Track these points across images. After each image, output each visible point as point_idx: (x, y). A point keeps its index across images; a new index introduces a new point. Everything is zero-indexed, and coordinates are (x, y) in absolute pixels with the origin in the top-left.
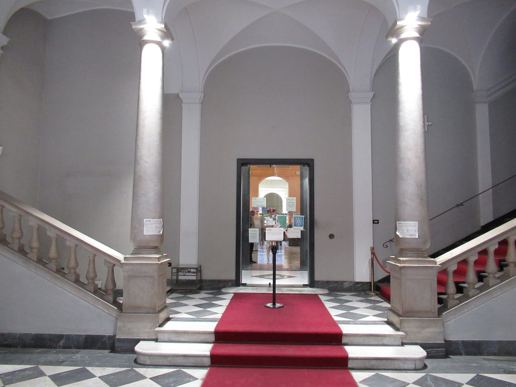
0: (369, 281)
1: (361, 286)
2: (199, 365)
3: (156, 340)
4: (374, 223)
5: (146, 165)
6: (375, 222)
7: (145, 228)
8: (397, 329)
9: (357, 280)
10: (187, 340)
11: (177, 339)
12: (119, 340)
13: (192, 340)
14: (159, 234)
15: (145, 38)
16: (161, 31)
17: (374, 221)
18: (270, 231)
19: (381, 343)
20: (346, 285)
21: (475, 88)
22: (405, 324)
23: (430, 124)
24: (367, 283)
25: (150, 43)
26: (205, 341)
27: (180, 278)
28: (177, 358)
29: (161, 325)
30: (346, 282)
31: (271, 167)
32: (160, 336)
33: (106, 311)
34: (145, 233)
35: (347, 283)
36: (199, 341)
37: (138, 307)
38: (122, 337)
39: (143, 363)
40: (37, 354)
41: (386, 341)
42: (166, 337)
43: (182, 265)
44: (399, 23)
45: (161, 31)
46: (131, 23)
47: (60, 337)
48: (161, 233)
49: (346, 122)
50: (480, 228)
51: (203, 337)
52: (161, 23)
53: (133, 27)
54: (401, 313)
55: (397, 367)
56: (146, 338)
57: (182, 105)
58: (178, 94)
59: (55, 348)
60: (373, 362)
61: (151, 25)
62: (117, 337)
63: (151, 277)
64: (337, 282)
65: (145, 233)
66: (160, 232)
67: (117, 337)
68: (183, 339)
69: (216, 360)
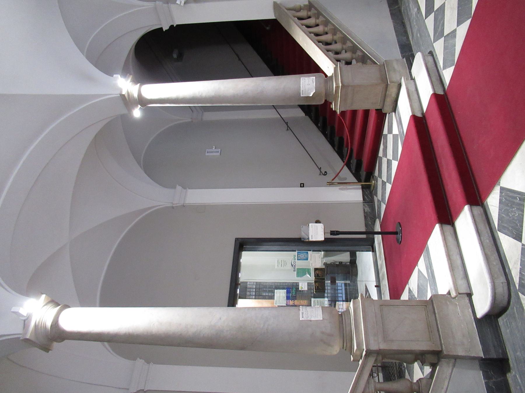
0: (361, 191)
1: (368, 197)
3: (470, 295)
4: (303, 187)
6: (302, 185)
7: (313, 319)
8: (400, 86)
9: (361, 199)
10: (458, 257)
11: (460, 268)
12: (485, 350)
13: (457, 250)
15: (49, 324)
17: (301, 187)
18: (313, 236)
19: (415, 92)
20: (367, 209)
21: (190, 120)
22: (394, 79)
23: (214, 147)
24: (363, 191)
25: (58, 318)
26: (454, 235)
28: (484, 244)
30: (364, 210)
31: (240, 284)
33: (446, 384)
34: (320, 318)
35: (366, 209)
36: (456, 243)
37: (429, 326)
39: (506, 288)
41: (412, 89)
42: (462, 283)
44: (124, 93)
49: (202, 209)
50: (307, 117)
51: (450, 239)
52: (41, 296)
54: (384, 85)
55: (433, 66)
60: (434, 79)
61: (37, 311)
62: (482, 355)
64: (365, 217)
65: (320, 318)
67: (482, 355)
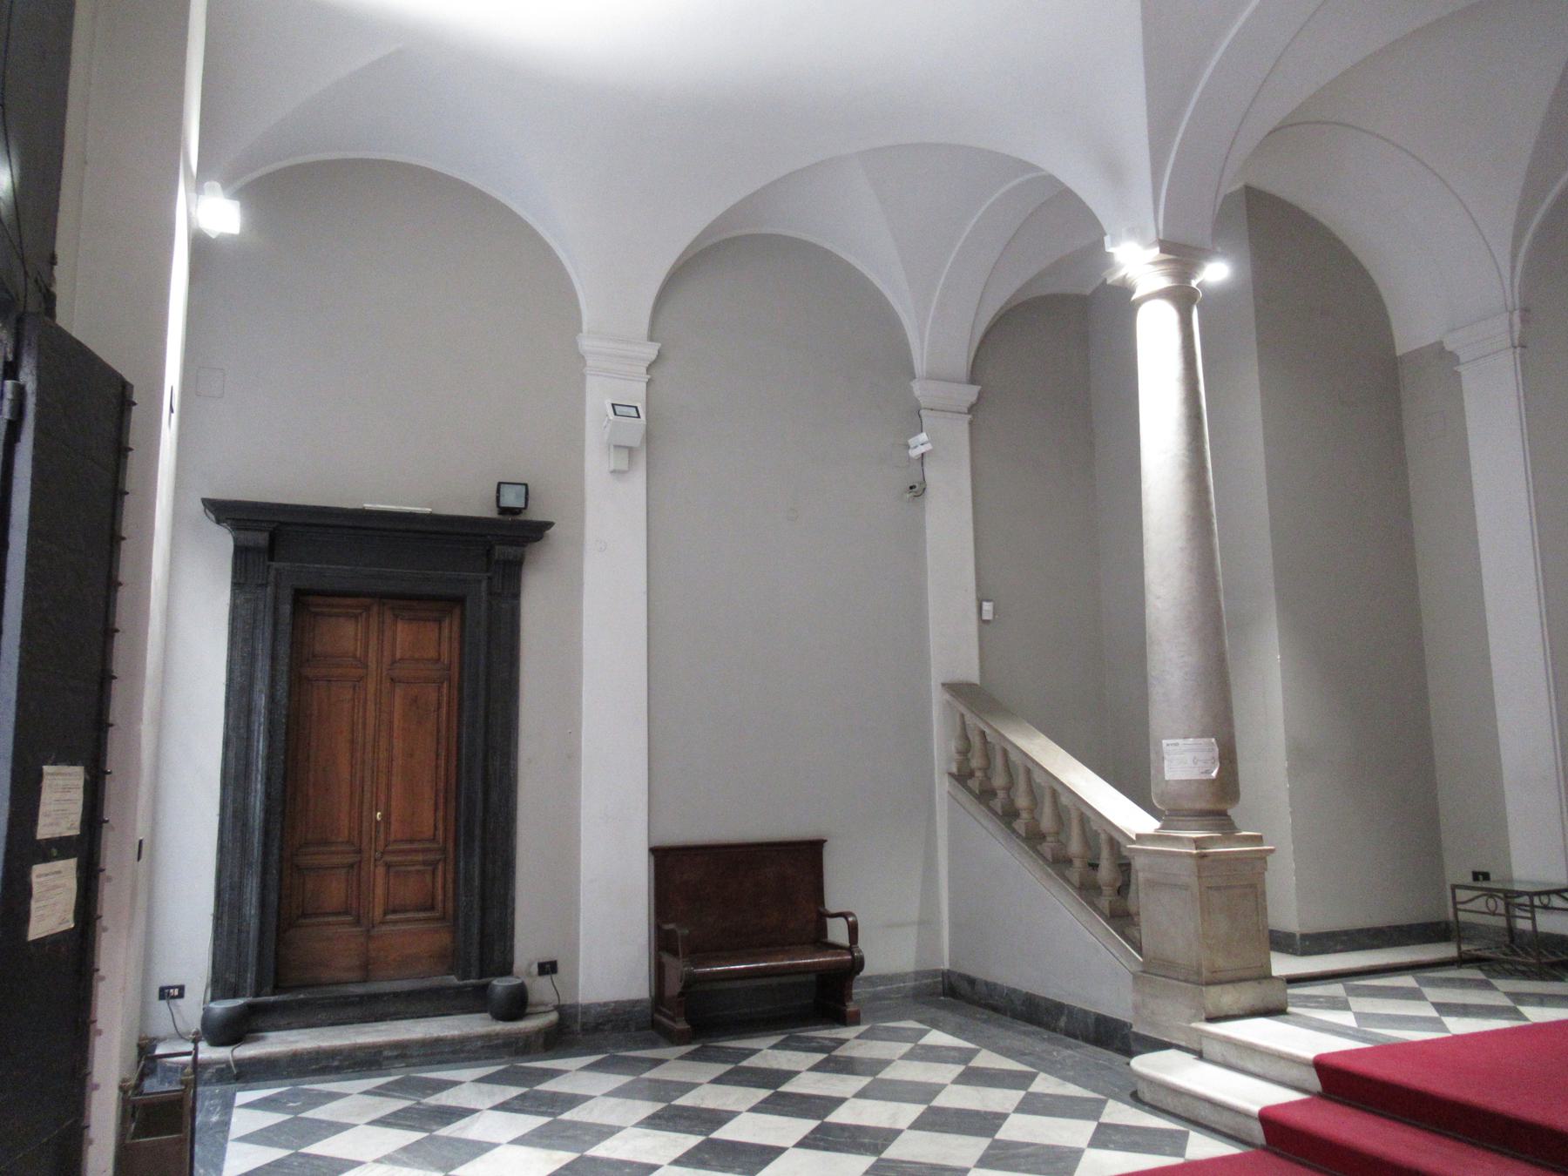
2: (1243, 1136)
5: (1159, 604)
11: (1241, 1063)
13: (1286, 1079)
14: (1204, 777)
16: (1155, 263)
27: (1523, 924)
29: (1211, 1019)
32: (1209, 1048)
38: (1142, 1032)
40: (1035, 1041)
43: (1521, 882)
45: (1155, 263)
46: (46, 768)
47: (1059, 1008)
48: (1214, 774)
52: (1148, 246)
53: (1109, 281)
56: (1183, 1044)
57: (1461, 369)
58: (1441, 343)
59: (1047, 1026)
61: (1136, 262)
63: (1186, 887)
66: (1208, 772)
68: (1250, 1066)
69: (1277, 1131)
